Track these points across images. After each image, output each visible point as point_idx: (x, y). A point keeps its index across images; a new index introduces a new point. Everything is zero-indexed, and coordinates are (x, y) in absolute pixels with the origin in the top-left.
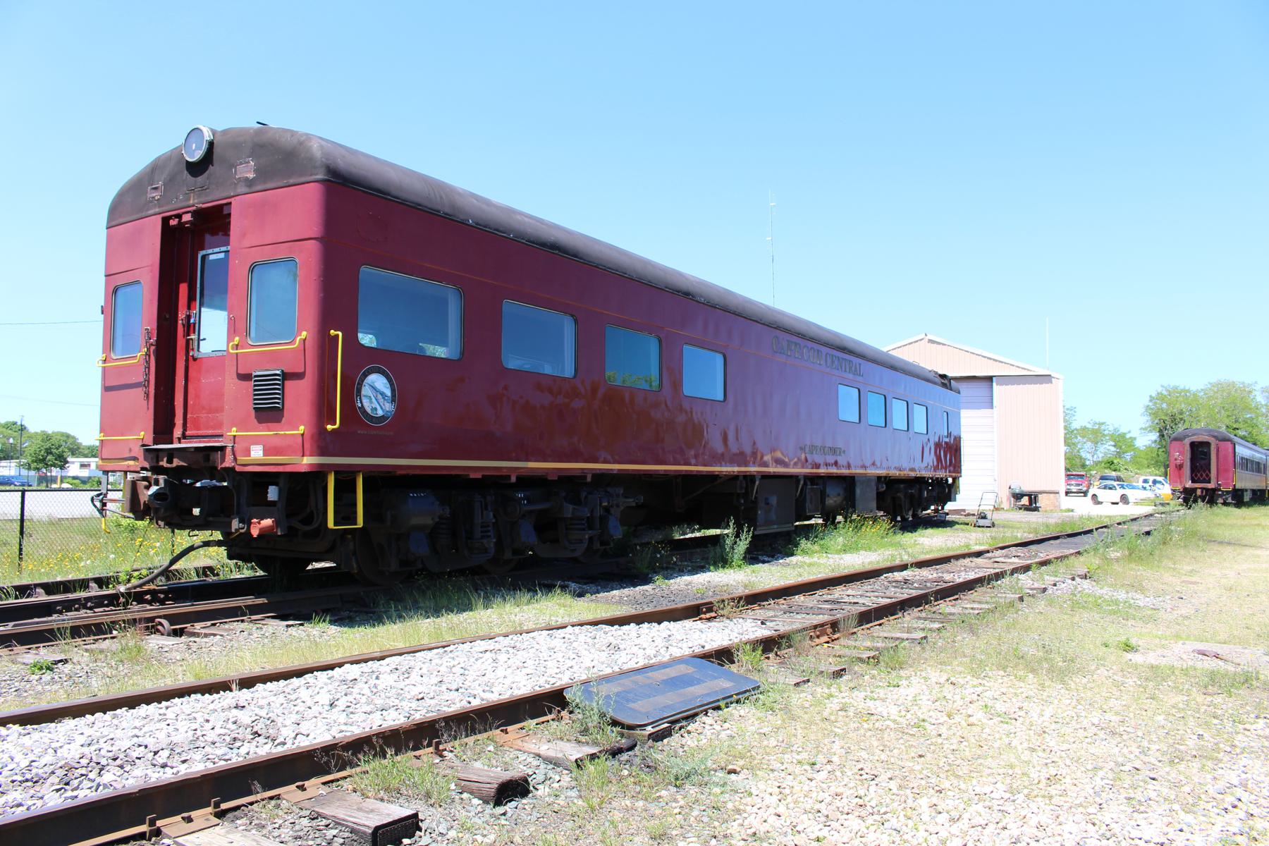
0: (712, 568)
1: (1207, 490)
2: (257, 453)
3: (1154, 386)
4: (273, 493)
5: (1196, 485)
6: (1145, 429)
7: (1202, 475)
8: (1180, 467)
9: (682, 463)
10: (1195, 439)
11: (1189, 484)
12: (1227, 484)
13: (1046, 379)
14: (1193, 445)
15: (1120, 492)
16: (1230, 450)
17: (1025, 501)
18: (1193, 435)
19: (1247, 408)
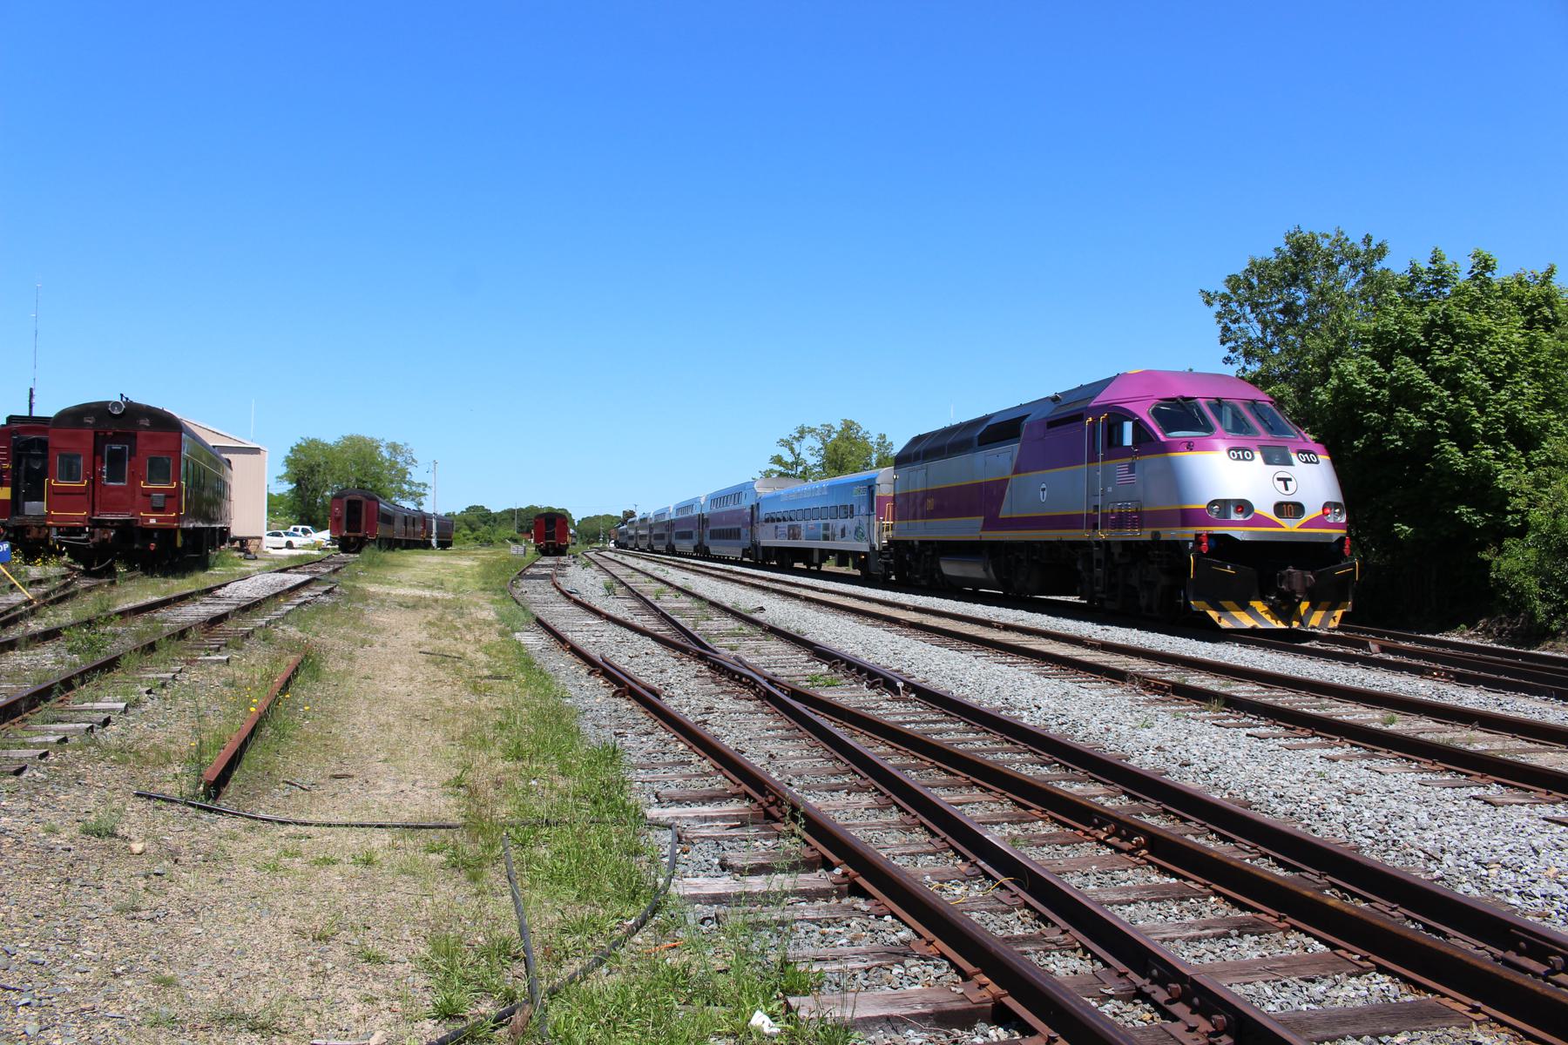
0: (916, 543)
2: (153, 521)
3: (294, 439)
4: (156, 535)
6: (281, 477)
8: (338, 520)
9: (551, 552)
10: (351, 497)
11: (345, 533)
13: (256, 451)
14: (349, 502)
15: (286, 539)
17: (237, 544)
19: (372, 464)
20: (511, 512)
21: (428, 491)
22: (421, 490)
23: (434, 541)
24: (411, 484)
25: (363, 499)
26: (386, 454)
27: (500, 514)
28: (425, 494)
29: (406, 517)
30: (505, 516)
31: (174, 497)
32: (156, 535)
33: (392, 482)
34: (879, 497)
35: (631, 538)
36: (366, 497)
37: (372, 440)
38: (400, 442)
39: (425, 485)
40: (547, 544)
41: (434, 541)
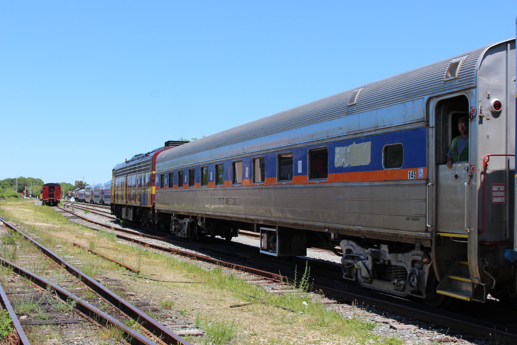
20: (7, 180)
30: (6, 182)
35: (87, 196)
40: (50, 200)
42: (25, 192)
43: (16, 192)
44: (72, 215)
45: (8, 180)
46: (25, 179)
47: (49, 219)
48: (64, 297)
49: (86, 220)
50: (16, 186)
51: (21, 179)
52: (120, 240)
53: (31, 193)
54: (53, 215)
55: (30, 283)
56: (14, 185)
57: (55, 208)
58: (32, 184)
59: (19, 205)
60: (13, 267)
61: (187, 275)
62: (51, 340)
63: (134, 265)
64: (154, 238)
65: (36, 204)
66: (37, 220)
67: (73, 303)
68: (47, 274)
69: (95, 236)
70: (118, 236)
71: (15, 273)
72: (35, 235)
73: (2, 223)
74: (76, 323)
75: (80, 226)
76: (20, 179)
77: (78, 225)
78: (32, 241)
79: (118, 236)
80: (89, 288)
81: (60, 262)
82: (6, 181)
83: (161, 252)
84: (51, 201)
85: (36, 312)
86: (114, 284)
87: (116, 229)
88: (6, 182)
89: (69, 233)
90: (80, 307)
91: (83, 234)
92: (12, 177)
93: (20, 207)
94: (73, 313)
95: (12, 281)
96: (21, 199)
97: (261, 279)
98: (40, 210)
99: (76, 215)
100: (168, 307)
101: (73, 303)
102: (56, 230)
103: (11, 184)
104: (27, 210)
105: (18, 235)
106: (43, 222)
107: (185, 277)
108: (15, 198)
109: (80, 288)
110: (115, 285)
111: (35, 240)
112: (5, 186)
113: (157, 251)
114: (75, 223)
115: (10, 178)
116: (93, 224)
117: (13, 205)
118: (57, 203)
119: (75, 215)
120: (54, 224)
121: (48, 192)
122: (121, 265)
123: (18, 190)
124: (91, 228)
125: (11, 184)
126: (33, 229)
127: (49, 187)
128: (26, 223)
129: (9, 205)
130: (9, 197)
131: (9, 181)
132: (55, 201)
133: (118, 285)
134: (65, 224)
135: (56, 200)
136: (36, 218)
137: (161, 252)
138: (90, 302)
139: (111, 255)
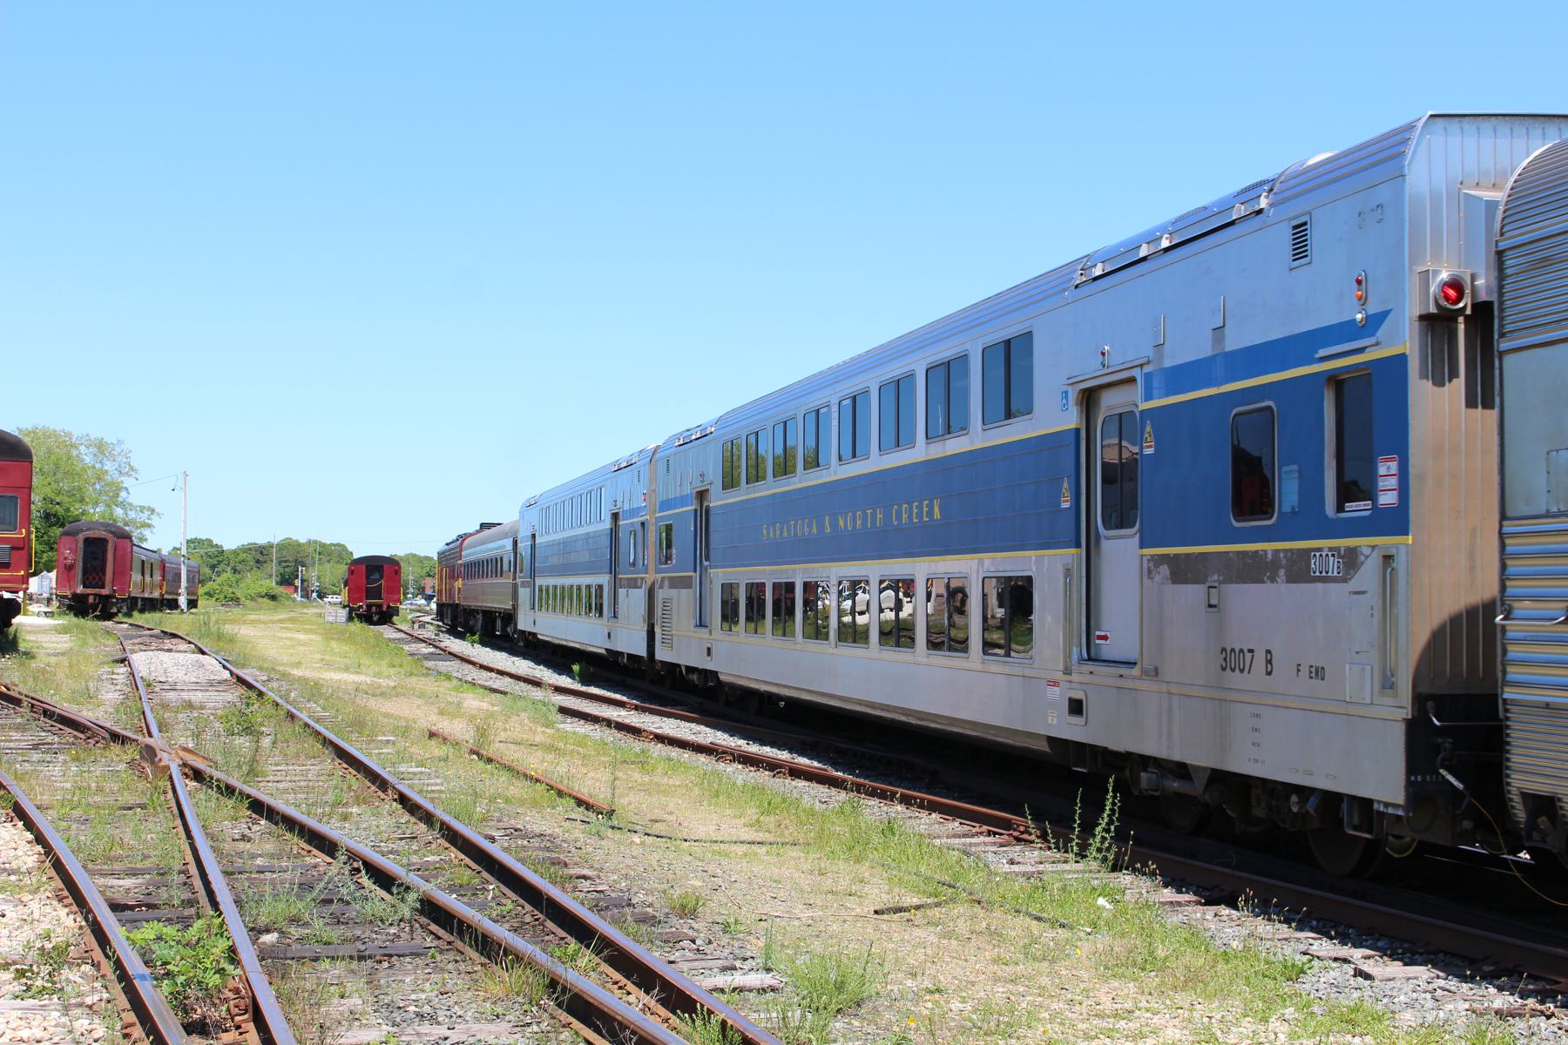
1: (100, 596)
5: (89, 591)
7: (94, 579)
10: (90, 534)
11: (80, 590)
12: (123, 591)
14: (87, 541)
16: (129, 550)
18: (87, 530)
20: (248, 549)
21: (155, 520)
22: (144, 517)
23: (183, 601)
24: (122, 505)
25: (110, 537)
26: (88, 460)
27: (235, 553)
28: (149, 526)
29: (143, 561)
30: (243, 556)
31: (22, 549)
32: (1413, 778)
33: (96, 504)
34: (1078, 546)
36: (112, 533)
37: (70, 435)
38: (110, 438)
39: (153, 511)
40: (369, 606)
41: (183, 601)
42: (298, 583)
43: (274, 584)
44: (432, 650)
45: (250, 549)
46: (299, 545)
47: (365, 661)
48: (384, 880)
49: (473, 663)
50: (274, 568)
51: (288, 546)
52: (569, 720)
53: (317, 586)
54: (378, 649)
55: (296, 843)
56: (265, 562)
57: (386, 631)
58: (320, 559)
59: (281, 621)
60: (249, 796)
61: (758, 821)
62: (343, 1001)
63: (601, 797)
64: (669, 715)
65: (331, 619)
66: (329, 665)
67: (412, 897)
68: (345, 818)
69: (495, 708)
70: (564, 711)
71: (254, 816)
72: (319, 709)
73: (227, 675)
74: (418, 955)
75: (455, 682)
76: (283, 545)
77: (448, 677)
78: (307, 725)
79: (564, 711)
80: (463, 857)
81: (382, 784)
82: (244, 552)
83: (687, 755)
84: (374, 609)
85: (306, 925)
86: (537, 845)
87: (559, 690)
88: (245, 555)
89: (420, 702)
90: (432, 911)
91: (459, 704)
92: (262, 540)
93: (282, 628)
94: (412, 927)
95: (244, 838)
96: (287, 603)
97: (977, 834)
98: (351, 639)
99: (444, 651)
100: (687, 911)
101: (412, 897)
102: (383, 694)
103: (258, 562)
104: (302, 637)
105: (270, 709)
106: (347, 669)
107: (751, 826)
108: (268, 601)
109: (436, 858)
110: (540, 849)
111: (318, 721)
112: (239, 567)
113: (675, 752)
114: (440, 673)
115: (255, 544)
116: (493, 675)
117: (264, 623)
118: (392, 616)
119: (441, 649)
120: (378, 675)
121: (365, 582)
122: (560, 793)
123: (278, 579)
124: (485, 688)
125: (258, 562)
126: (314, 690)
127: (367, 566)
128: (296, 672)
129: (252, 622)
130: (252, 599)
131: (253, 553)
132: (385, 608)
133: (548, 849)
134: (411, 674)
135: (389, 607)
136: (327, 657)
137: (686, 755)
138: (462, 895)
139: (535, 763)
